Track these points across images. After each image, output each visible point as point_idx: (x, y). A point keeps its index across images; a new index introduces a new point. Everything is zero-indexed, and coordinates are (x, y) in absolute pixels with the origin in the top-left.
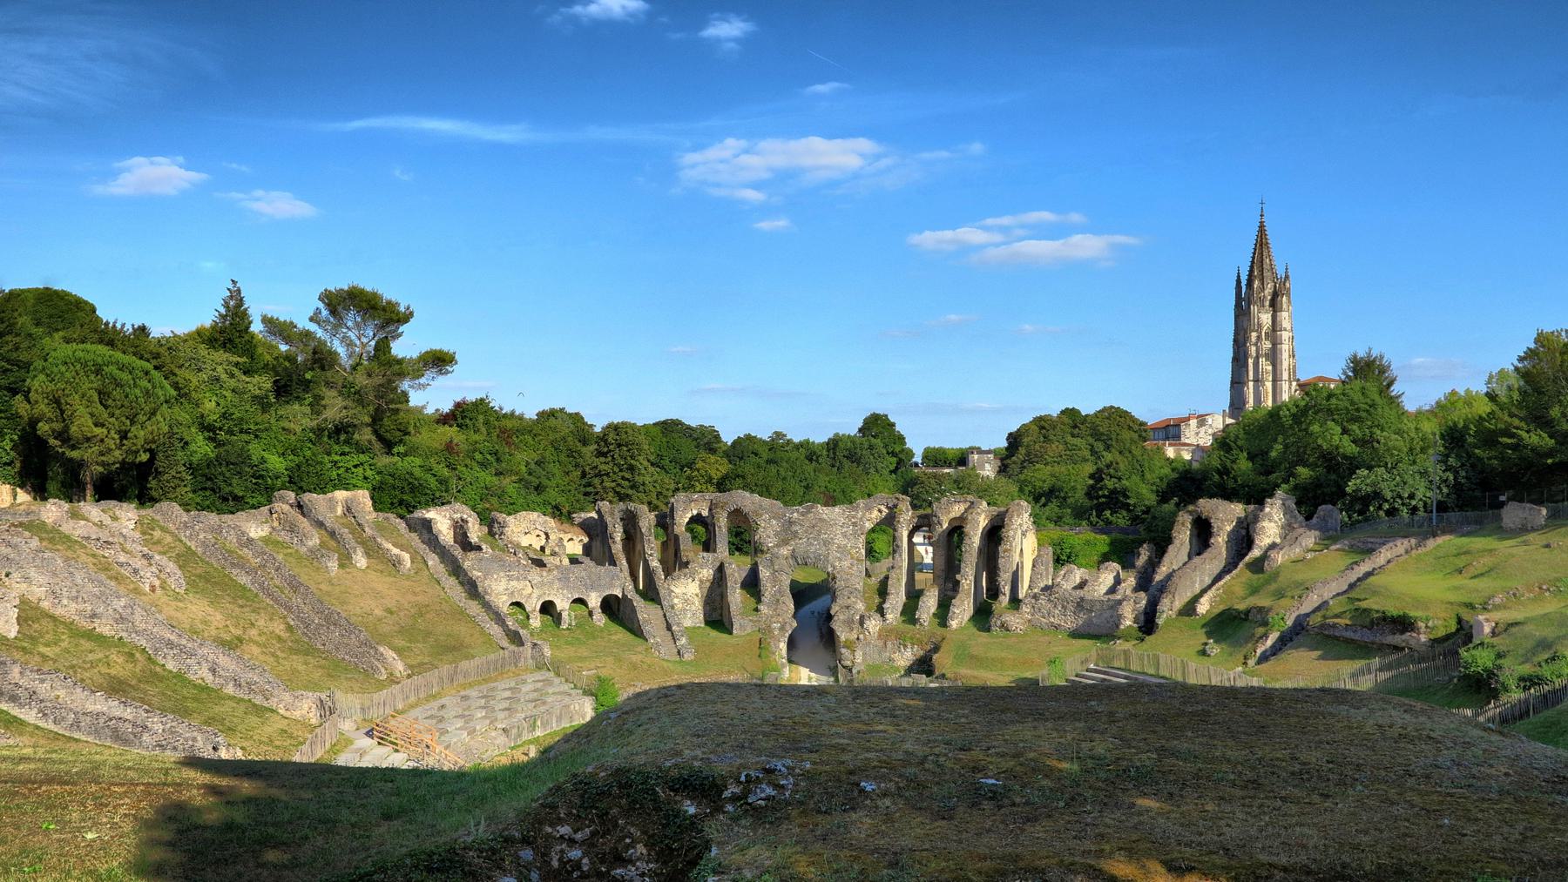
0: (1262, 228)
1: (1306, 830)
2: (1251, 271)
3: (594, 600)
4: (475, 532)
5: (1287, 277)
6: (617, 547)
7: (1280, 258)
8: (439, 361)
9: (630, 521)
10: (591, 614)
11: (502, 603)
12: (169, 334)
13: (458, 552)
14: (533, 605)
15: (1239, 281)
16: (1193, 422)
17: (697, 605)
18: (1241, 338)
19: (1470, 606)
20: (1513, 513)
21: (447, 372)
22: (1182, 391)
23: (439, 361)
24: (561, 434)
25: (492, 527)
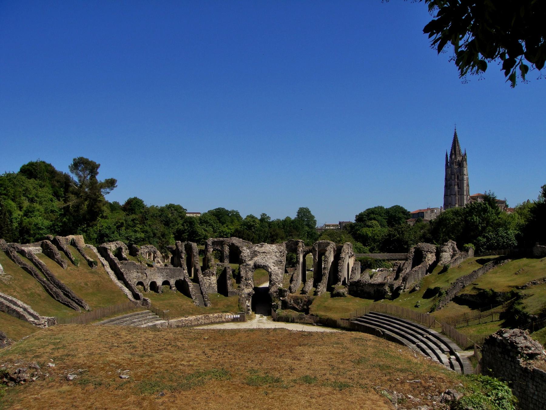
0: (455, 132)
1: (376, 222)
2: (452, 151)
3: (172, 282)
4: (125, 254)
5: (465, 154)
6: (184, 262)
7: (463, 147)
8: (111, 183)
9: (189, 249)
10: (171, 288)
11: (133, 282)
12: (12, 172)
13: (117, 261)
14: (147, 283)
15: (447, 155)
16: (429, 211)
17: (215, 286)
18: (448, 177)
19: (517, 287)
20: (339, 268)
21: (116, 186)
22: (425, 197)
23: (111, 183)
24: (171, 216)
25: (133, 252)
